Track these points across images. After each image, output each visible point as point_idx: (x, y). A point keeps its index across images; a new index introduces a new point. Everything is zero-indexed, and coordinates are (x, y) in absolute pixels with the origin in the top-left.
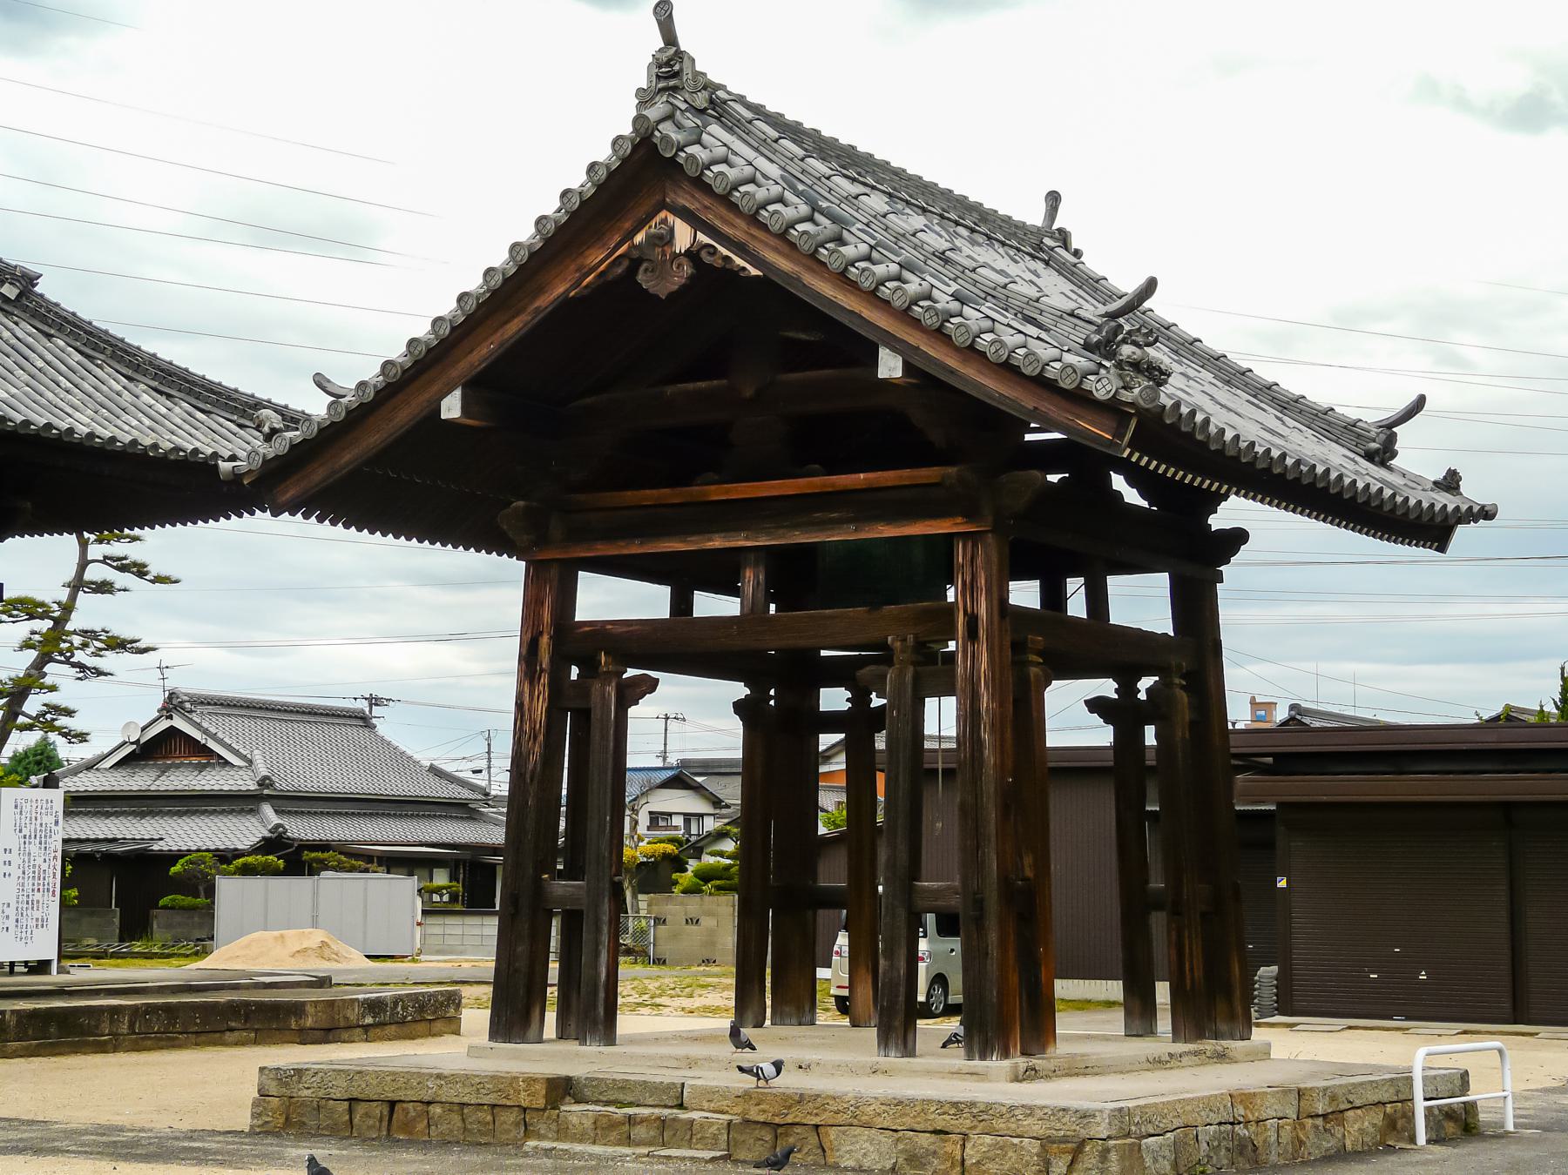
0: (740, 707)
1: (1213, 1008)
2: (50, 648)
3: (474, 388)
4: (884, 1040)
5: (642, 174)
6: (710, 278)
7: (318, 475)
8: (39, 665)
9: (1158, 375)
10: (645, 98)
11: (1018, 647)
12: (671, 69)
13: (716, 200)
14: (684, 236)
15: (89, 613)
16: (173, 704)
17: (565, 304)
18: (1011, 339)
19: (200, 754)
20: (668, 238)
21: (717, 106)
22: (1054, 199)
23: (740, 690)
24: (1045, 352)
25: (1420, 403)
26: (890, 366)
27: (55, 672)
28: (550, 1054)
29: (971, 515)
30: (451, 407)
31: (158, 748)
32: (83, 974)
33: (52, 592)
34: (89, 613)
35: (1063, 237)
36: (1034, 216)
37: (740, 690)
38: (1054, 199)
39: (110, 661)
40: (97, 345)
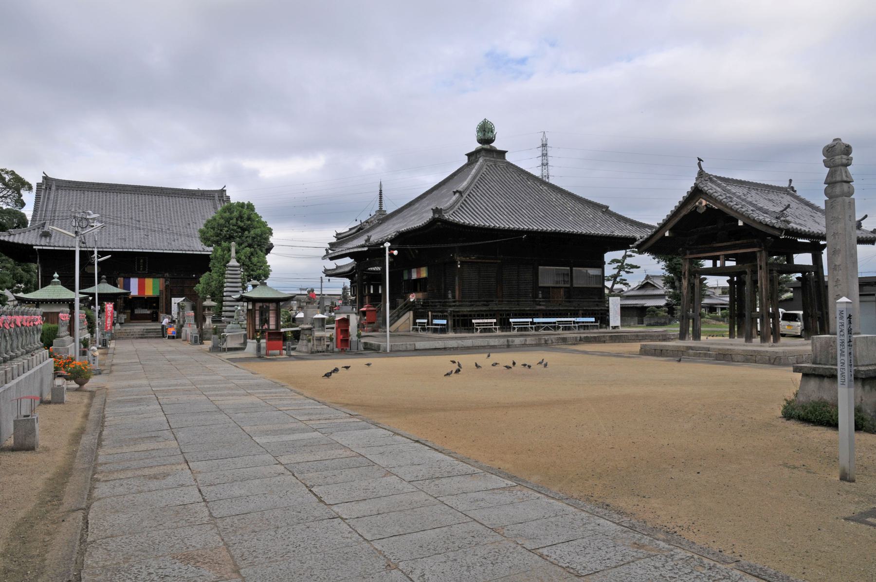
0: (728, 281)
1: (456, 333)
2: (621, 268)
3: (671, 230)
4: (746, 341)
5: (696, 192)
6: (709, 209)
7: (645, 247)
8: (619, 272)
9: (789, 222)
10: (697, 179)
11: (771, 271)
12: (701, 174)
13: (708, 197)
14: (704, 203)
15: (628, 261)
16: (648, 277)
17: (685, 216)
18: (761, 218)
19: (653, 286)
20: (701, 203)
21: (710, 178)
22: (791, 181)
23: (728, 278)
24: (767, 220)
25: (866, 216)
26: (740, 223)
27: (622, 273)
28: (689, 342)
29: (760, 247)
30: (667, 234)
31: (645, 286)
32: (621, 329)
33: (620, 258)
34: (628, 261)
35: (792, 188)
36: (785, 184)
37: (728, 278)
38: (791, 181)
39: (631, 270)
40: (621, 218)
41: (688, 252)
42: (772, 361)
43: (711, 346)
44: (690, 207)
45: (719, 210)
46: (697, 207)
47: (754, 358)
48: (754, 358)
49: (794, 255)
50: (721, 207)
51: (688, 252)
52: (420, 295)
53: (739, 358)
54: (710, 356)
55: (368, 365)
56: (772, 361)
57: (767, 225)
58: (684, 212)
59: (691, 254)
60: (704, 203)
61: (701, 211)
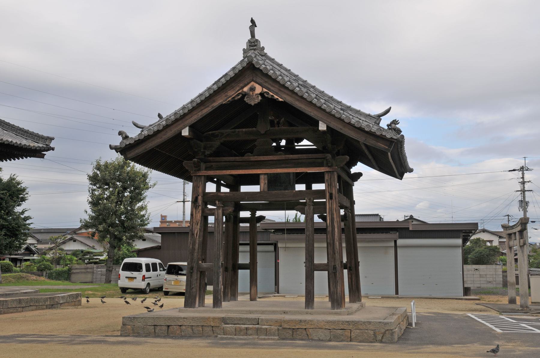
3: (192, 127)
6: (267, 102)
12: (253, 44)
20: (253, 89)
30: (185, 132)
41: (203, 165)
42: (379, 337)
43: (263, 317)
44: (232, 94)
45: (284, 103)
46: (244, 95)
47: (347, 333)
48: (347, 333)
49: (305, 185)
50: (289, 99)
51: (203, 165)
52: (321, 123)
53: (321, 334)
54: (267, 332)
55: (494, 351)
56: (379, 337)
57: (361, 129)
58: (220, 101)
59: (207, 169)
60: (259, 89)
61: (254, 101)
